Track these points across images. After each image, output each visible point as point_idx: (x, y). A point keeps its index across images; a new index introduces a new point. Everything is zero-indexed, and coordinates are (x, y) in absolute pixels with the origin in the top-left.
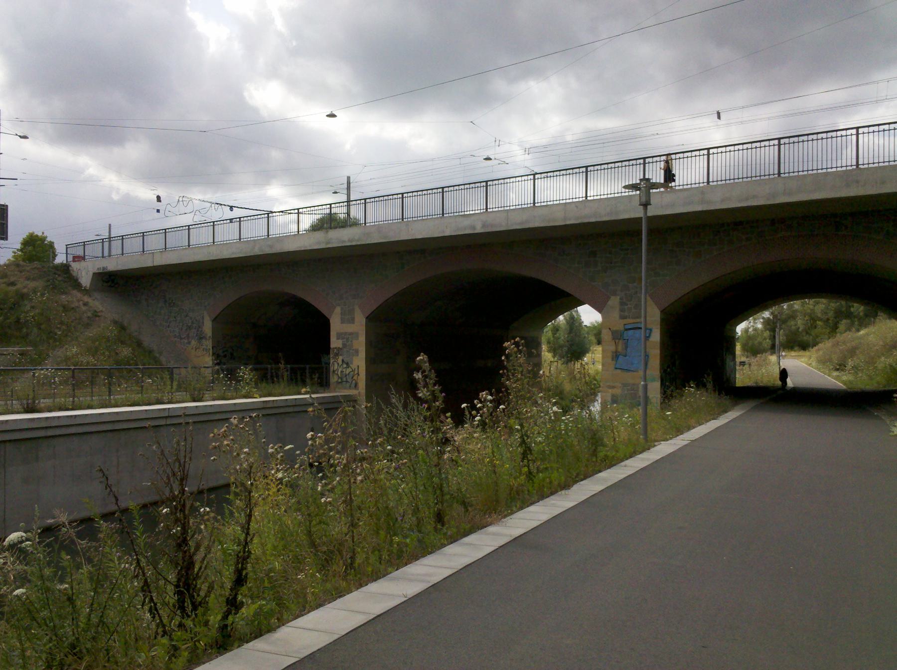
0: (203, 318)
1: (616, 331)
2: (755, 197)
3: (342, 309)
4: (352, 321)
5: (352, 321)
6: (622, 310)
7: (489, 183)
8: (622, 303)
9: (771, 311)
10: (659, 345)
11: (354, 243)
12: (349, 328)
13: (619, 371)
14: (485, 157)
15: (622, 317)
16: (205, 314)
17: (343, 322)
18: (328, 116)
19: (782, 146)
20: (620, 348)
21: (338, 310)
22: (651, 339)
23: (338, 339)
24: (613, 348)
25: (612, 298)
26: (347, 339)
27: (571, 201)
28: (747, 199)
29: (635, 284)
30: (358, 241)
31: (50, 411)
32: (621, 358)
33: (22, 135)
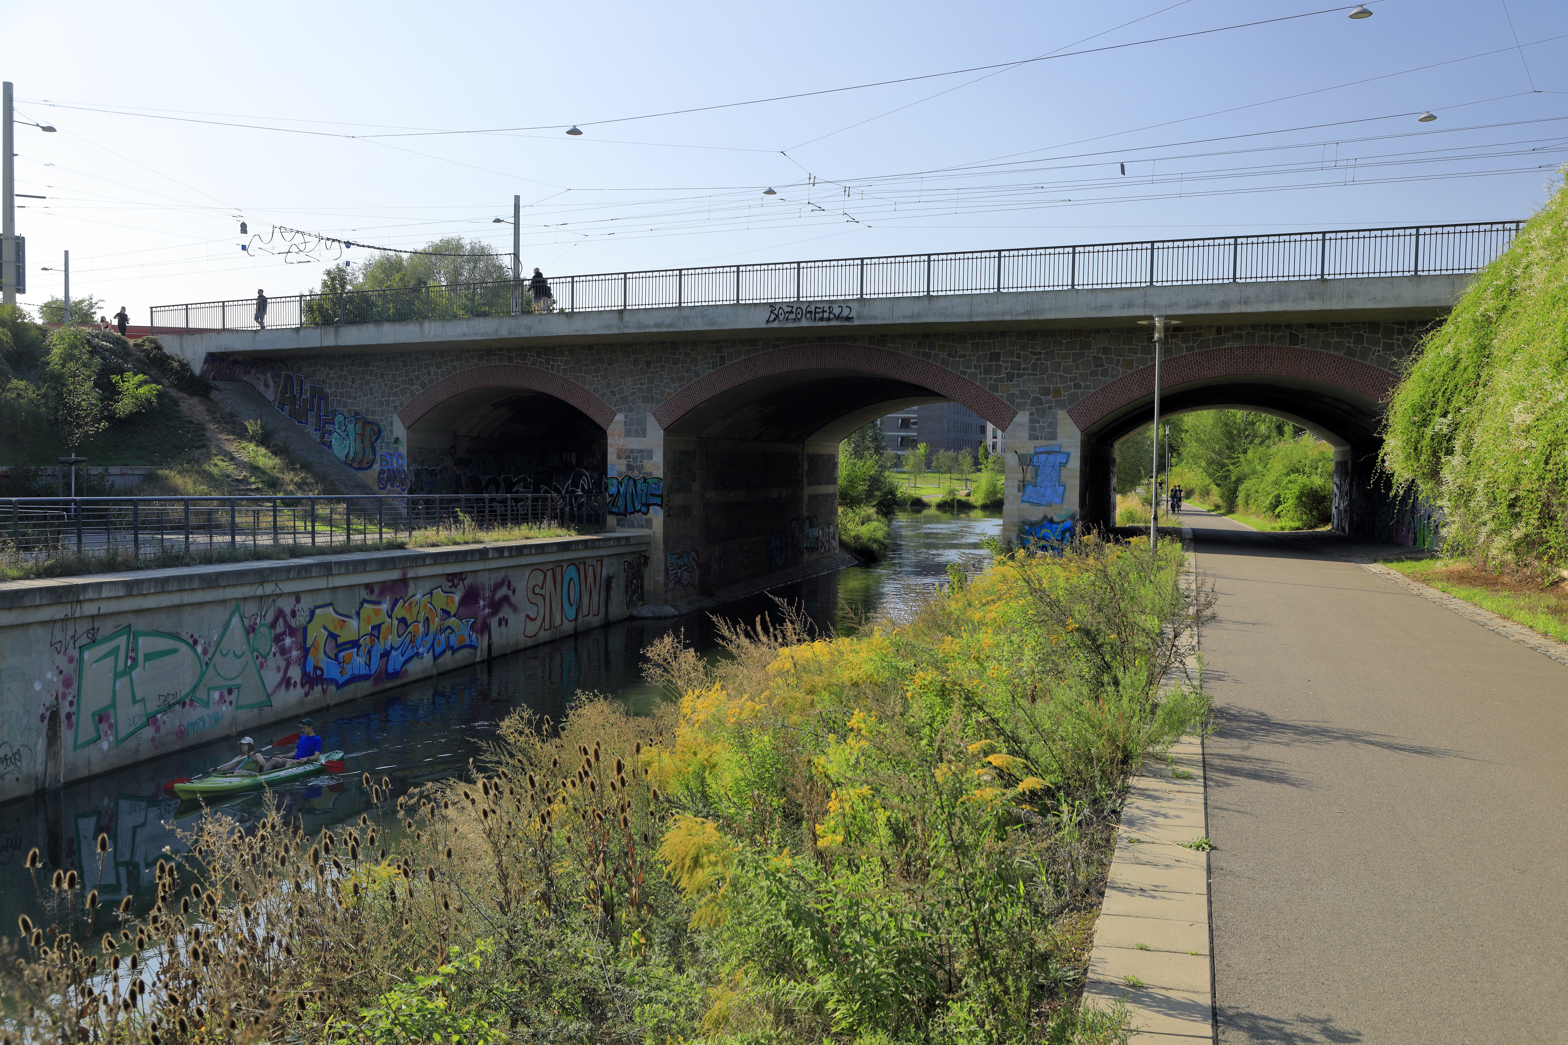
0: (391, 424)
1: (1025, 456)
2: (1207, 304)
3: (626, 416)
4: (643, 433)
5: (643, 433)
6: (1032, 429)
7: (865, 261)
8: (1032, 421)
9: (526, 283)
10: (1078, 474)
11: (664, 330)
12: (635, 443)
13: (1027, 505)
14: (568, 129)
15: (1033, 437)
16: (396, 417)
17: (628, 434)
18: (569, 132)
19: (1239, 247)
20: (1029, 477)
21: (620, 417)
22: (1069, 466)
23: (619, 457)
24: (1020, 476)
25: (1020, 413)
26: (635, 458)
27: (978, 292)
28: (1196, 306)
29: (1050, 397)
30: (670, 326)
31: (271, 570)
32: (1029, 489)
33: (45, 125)
